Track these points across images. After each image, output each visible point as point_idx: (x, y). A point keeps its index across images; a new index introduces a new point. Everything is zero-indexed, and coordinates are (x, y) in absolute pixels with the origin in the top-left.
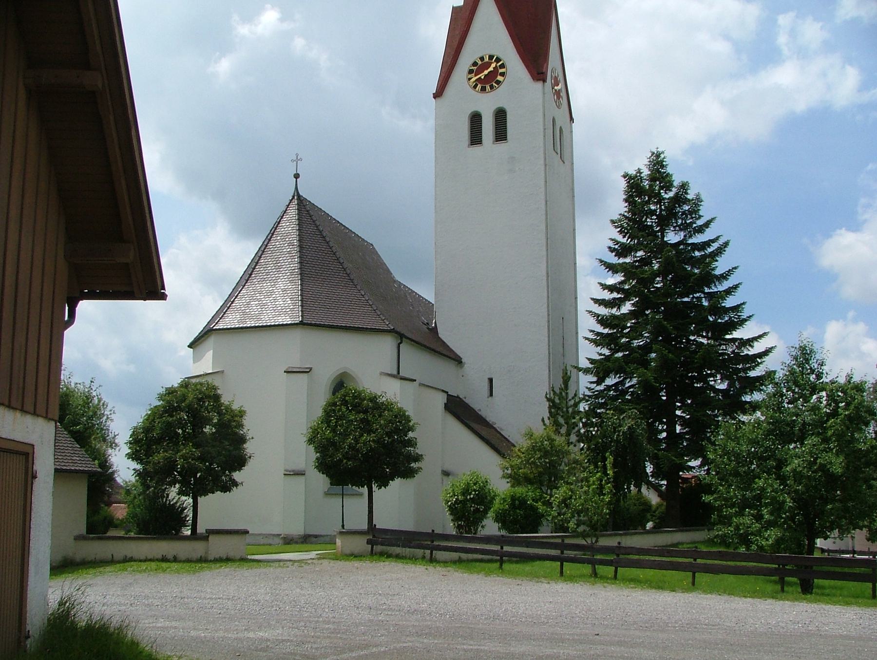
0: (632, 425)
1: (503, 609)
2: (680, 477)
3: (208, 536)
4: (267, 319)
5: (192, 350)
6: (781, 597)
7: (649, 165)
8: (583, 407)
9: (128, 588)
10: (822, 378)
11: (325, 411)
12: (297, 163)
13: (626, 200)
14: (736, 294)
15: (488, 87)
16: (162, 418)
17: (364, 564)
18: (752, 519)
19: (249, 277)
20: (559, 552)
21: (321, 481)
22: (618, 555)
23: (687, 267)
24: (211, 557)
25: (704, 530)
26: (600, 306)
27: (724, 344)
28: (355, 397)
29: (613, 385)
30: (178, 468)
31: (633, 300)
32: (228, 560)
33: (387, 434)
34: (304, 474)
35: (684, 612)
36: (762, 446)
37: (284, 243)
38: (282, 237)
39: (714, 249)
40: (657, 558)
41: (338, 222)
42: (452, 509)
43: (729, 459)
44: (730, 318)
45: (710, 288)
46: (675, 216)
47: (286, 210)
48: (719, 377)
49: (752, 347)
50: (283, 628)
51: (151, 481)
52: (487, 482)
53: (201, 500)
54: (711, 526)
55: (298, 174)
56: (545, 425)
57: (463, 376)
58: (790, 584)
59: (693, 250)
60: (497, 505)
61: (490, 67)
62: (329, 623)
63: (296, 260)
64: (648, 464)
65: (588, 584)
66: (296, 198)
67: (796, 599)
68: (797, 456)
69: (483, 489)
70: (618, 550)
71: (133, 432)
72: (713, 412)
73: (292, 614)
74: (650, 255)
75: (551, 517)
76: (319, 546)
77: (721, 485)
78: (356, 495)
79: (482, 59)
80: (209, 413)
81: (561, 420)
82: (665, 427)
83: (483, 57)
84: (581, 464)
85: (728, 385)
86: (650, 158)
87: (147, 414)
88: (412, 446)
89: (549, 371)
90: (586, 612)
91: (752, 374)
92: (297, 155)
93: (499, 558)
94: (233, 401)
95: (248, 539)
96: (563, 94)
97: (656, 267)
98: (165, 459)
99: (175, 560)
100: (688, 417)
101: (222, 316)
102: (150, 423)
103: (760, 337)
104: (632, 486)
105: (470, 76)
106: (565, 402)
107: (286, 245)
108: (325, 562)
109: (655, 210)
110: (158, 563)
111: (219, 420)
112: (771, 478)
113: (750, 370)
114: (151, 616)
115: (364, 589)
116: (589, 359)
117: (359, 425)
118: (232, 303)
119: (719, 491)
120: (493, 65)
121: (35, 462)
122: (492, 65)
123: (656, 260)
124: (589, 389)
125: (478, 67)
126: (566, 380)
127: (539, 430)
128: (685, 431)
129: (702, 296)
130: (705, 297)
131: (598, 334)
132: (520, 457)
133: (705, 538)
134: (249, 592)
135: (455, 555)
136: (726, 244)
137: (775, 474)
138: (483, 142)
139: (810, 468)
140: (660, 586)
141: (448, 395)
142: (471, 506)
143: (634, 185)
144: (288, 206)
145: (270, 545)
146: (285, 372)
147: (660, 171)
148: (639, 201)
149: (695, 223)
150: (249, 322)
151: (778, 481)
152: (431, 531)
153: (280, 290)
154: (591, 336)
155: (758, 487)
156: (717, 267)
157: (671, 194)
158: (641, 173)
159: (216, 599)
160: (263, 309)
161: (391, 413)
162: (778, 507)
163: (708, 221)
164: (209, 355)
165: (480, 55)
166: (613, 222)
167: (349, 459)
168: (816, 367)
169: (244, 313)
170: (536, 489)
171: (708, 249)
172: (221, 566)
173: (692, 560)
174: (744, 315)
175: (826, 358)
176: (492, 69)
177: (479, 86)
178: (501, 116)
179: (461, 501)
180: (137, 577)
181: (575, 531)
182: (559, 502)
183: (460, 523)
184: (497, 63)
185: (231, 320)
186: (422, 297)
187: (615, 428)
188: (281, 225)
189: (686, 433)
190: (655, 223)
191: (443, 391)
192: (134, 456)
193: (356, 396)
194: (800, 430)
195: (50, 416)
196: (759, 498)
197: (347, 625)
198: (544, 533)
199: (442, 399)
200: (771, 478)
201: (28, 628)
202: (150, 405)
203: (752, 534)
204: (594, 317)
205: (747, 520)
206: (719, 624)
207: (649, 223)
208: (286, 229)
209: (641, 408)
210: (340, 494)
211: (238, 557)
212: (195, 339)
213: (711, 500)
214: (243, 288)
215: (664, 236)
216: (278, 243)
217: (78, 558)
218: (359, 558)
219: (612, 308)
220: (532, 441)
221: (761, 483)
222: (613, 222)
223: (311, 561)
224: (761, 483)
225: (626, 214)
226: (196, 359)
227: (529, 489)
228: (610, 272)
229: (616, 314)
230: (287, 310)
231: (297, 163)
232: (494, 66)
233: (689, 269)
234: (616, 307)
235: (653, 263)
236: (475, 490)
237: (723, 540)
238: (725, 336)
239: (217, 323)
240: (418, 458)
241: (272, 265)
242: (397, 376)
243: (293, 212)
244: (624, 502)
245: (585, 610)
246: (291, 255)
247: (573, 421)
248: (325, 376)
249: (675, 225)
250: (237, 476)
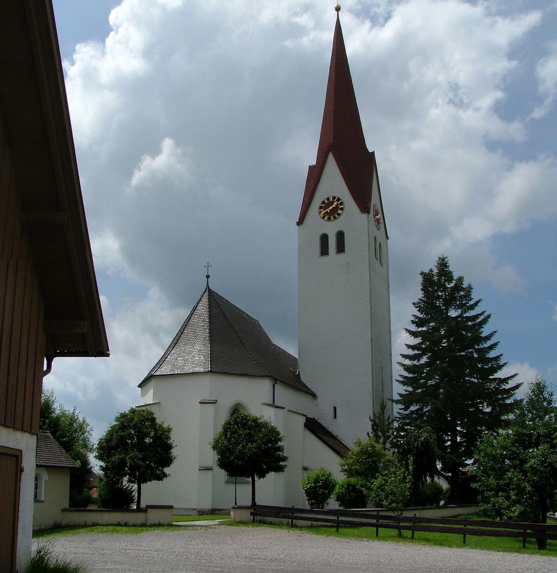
0: (427, 437)
1: (334, 559)
2: (460, 471)
3: (147, 510)
4: (189, 369)
5: (140, 388)
6: (523, 552)
7: (438, 266)
8: (396, 424)
9: (93, 543)
10: (551, 404)
11: (224, 428)
12: (208, 268)
13: (422, 290)
14: (496, 349)
15: (332, 218)
16: (117, 432)
17: (248, 528)
18: (504, 499)
19: (177, 342)
20: (376, 520)
21: (222, 474)
22: (414, 523)
23: (463, 332)
24: (148, 523)
25: (472, 506)
26: (406, 359)
27: (488, 382)
28: (243, 419)
29: (415, 411)
30: (128, 466)
31: (428, 355)
32: (160, 525)
33: (264, 443)
34: (212, 469)
35: (455, 561)
36: (510, 450)
37: (199, 320)
38: (198, 316)
39: (481, 320)
40: (441, 525)
41: (235, 306)
42: (308, 492)
43: (488, 459)
44: (492, 365)
45: (478, 345)
46: (455, 299)
47: (201, 299)
48: (485, 404)
49: (507, 383)
50: (186, 570)
51: (110, 473)
52: (330, 474)
53: (143, 486)
54: (475, 503)
55: (209, 276)
56: (369, 437)
57: (317, 405)
58: (531, 543)
59: (467, 321)
60: (337, 489)
61: (333, 204)
62: (217, 567)
63: (207, 331)
64: (438, 462)
65: (394, 542)
66: (207, 291)
67: (533, 553)
68: (533, 457)
69: (328, 479)
70: (414, 520)
71: (100, 442)
72: (481, 428)
73: (194, 561)
74: (439, 325)
75: (371, 497)
76: (221, 516)
77: (483, 476)
78: (246, 483)
79: (328, 199)
80: (148, 429)
81: (380, 434)
82: (450, 437)
83: (329, 198)
84: (393, 463)
85: (491, 409)
86: (437, 262)
87: (108, 430)
88: (281, 451)
89: (373, 402)
90: (389, 561)
91: (508, 401)
92: (208, 263)
93: (336, 524)
94: (164, 422)
95: (174, 511)
96: (381, 221)
97: (443, 333)
98: (119, 459)
99: (126, 525)
100: (465, 431)
101: (159, 367)
102: (110, 436)
103: (513, 376)
104: (428, 477)
105: (320, 211)
106: (382, 422)
107: (201, 321)
108: (223, 527)
109: (442, 296)
110: (115, 527)
111: (155, 434)
112: (516, 471)
113: (507, 399)
114: (103, 562)
115: (246, 545)
116: (399, 394)
117: (245, 437)
118: (166, 358)
119: (482, 480)
120: (336, 203)
121: (22, 461)
122: (335, 203)
123: (442, 328)
124: (399, 413)
125: (326, 204)
126: (383, 407)
127: (365, 440)
128: (463, 440)
129: (474, 351)
130: (475, 352)
131: (405, 377)
132: (352, 458)
133: (473, 512)
134: (170, 546)
135: (309, 523)
136: (489, 316)
137: (519, 469)
138: (329, 253)
139: (542, 465)
140: (441, 543)
141: (307, 417)
142: (320, 491)
143: (427, 279)
144: (202, 296)
145: (190, 515)
146: (199, 403)
147: (445, 270)
148: (431, 290)
149: (468, 304)
150: (176, 371)
151: (521, 474)
152: (292, 507)
153: (197, 350)
154: (401, 379)
155: (508, 477)
156: (483, 332)
157: (452, 285)
158: (432, 271)
159: (147, 550)
160: (186, 363)
161: (266, 429)
162: (521, 491)
163: (477, 302)
164: (151, 392)
165: (327, 197)
166: (414, 304)
167: (239, 460)
168: (547, 397)
169: (173, 365)
170: (363, 479)
171: (477, 320)
172: (155, 529)
173: (464, 526)
174: (501, 362)
175: (554, 391)
176: (335, 206)
177: (326, 217)
178: (340, 236)
179: (313, 487)
180: (100, 536)
181: (387, 507)
182: (376, 488)
183: (312, 501)
184: (338, 202)
185: (165, 370)
186: (291, 355)
187: (415, 439)
188: (197, 308)
189: (464, 442)
190: (442, 304)
191: (303, 415)
192: (100, 457)
193: (244, 419)
194: (535, 439)
195: (33, 431)
196: (508, 485)
197: (229, 568)
198: (370, 508)
199: (303, 420)
200: (516, 471)
201: (17, 568)
202: (111, 424)
203: (504, 509)
204: (400, 365)
205: (500, 500)
206: (477, 570)
207: (437, 304)
208: (201, 311)
209: (433, 426)
210: (234, 483)
211: (166, 523)
212: (142, 381)
213: (476, 487)
214: (172, 349)
215: (448, 312)
216: (195, 320)
217: (64, 523)
218: (246, 524)
219: (414, 361)
220: (361, 448)
221: (509, 474)
222: (414, 304)
223: (214, 526)
224: (509, 474)
225: (423, 298)
226: (143, 394)
227: (358, 479)
228: (413, 337)
229: (417, 364)
230: (201, 363)
231: (208, 268)
232: (336, 204)
233: (465, 333)
234: (417, 360)
235: (441, 330)
236: (322, 480)
237: (485, 513)
238: (489, 377)
239: (156, 371)
240: (284, 459)
241: (191, 334)
242: (273, 405)
243: (205, 300)
244: (422, 487)
245: (389, 560)
246: (204, 328)
247: (388, 434)
248: (226, 405)
249: (455, 305)
250: (166, 470)
